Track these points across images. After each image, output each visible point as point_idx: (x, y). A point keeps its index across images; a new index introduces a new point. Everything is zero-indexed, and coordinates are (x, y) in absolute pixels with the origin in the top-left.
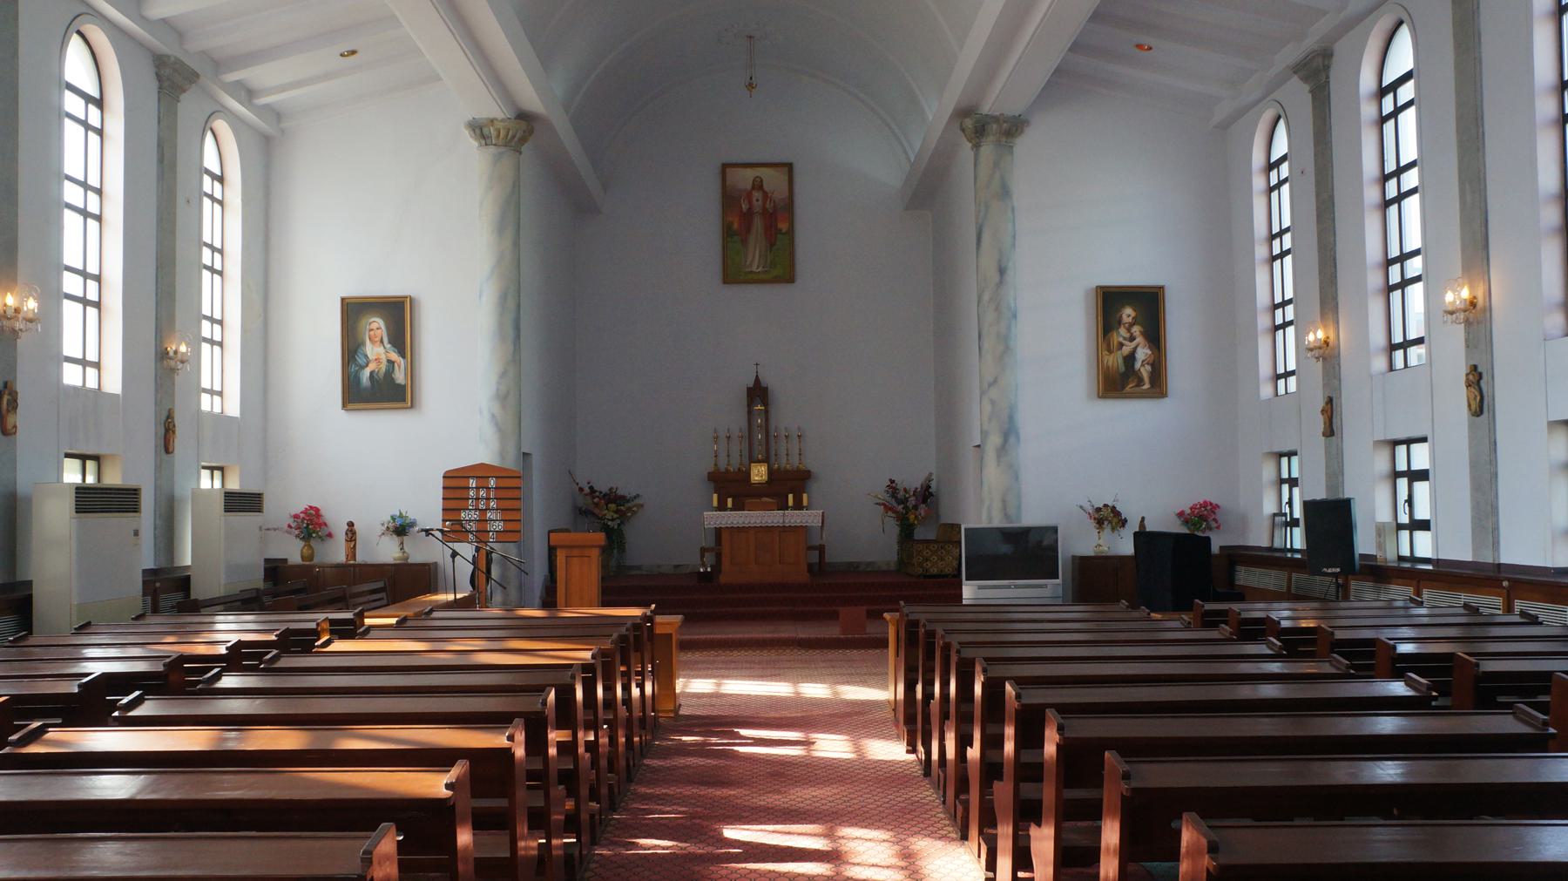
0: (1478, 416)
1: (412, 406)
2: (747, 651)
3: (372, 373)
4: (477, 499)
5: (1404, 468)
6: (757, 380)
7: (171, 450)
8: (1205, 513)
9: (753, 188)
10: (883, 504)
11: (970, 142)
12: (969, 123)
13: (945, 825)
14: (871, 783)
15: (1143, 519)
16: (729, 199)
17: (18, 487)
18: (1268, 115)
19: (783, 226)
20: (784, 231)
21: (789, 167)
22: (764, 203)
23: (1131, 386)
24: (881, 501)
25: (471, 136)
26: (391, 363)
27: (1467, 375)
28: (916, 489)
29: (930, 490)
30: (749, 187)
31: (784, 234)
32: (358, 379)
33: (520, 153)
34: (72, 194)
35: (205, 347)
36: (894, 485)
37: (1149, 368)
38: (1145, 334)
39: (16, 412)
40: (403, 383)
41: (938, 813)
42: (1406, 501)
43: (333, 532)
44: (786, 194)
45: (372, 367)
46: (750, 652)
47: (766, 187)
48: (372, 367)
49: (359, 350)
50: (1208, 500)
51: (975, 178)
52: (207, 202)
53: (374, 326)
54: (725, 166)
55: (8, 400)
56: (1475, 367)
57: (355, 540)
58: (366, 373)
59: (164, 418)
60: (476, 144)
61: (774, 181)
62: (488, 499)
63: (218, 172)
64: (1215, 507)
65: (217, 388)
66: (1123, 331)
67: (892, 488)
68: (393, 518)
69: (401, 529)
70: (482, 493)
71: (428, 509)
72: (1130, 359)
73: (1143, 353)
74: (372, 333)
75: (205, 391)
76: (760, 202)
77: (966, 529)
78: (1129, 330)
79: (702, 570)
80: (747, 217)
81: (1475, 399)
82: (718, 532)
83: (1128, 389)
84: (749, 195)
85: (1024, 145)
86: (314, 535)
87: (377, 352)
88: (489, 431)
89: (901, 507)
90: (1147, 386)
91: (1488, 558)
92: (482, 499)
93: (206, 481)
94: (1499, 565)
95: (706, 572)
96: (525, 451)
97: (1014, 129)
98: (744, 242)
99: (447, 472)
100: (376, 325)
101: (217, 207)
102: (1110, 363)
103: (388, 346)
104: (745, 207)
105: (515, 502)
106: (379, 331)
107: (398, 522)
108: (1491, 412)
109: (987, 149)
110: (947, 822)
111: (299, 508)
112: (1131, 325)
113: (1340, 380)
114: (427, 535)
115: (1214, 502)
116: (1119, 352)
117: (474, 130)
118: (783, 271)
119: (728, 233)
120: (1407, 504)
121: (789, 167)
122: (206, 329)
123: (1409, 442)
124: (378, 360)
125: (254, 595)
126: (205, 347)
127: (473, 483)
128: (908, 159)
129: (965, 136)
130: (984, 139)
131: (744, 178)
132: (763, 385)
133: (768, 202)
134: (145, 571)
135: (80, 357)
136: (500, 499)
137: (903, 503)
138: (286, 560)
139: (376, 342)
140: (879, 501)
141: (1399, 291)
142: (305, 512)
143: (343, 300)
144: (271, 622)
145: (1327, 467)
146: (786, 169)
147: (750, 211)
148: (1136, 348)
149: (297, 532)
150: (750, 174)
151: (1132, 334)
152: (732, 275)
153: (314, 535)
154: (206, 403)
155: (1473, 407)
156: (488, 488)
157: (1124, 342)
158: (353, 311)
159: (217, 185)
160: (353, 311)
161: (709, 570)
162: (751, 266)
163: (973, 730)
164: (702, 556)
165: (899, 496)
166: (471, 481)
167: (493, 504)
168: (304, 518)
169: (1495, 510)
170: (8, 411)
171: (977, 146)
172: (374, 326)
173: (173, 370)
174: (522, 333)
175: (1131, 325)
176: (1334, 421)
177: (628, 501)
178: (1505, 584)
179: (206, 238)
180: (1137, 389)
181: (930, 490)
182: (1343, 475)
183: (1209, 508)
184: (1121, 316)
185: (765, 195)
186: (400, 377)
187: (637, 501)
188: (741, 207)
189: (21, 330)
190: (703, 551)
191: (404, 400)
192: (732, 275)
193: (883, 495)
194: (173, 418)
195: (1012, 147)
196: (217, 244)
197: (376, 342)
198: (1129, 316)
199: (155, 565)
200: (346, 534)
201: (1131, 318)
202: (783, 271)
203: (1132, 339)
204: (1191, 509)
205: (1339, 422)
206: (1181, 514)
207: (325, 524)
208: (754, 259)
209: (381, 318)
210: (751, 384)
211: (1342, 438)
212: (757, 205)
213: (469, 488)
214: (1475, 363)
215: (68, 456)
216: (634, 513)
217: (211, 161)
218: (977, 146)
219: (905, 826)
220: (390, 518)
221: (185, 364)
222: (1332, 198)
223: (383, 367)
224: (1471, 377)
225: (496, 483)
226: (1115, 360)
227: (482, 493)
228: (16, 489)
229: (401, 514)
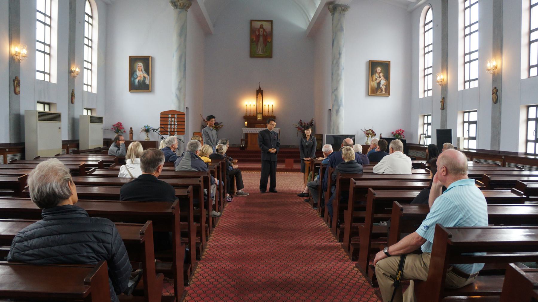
0: (496, 103)
1: (150, 92)
2: (256, 172)
3: (139, 80)
4: (171, 121)
5: (467, 120)
6: (260, 88)
7: (73, 102)
8: (400, 133)
9: (260, 28)
10: (298, 127)
11: (331, 13)
12: (331, 6)
13: (332, 236)
14: (303, 219)
15: (381, 134)
16: (253, 31)
17: (21, 110)
18: (426, 7)
19: (269, 40)
20: (269, 41)
21: (272, 21)
22: (263, 33)
23: (379, 92)
24: (297, 127)
25: (172, 6)
26: (144, 77)
27: (493, 90)
28: (308, 123)
29: (312, 124)
30: (259, 27)
31: (269, 42)
32: (134, 82)
33: (187, 11)
34: (39, 16)
35: (85, 70)
36: (301, 122)
37: (385, 87)
38: (384, 76)
39: (19, 87)
40: (148, 84)
41: (329, 231)
42: (534, 131)
43: (126, 130)
44: (270, 30)
45: (139, 78)
46: (254, 172)
47: (264, 28)
48: (139, 78)
49: (135, 73)
50: (401, 129)
51: (332, 24)
52: (86, 23)
53: (140, 65)
54: (252, 21)
55: (17, 83)
56: (495, 88)
57: (132, 133)
58: (137, 81)
59: (71, 92)
60: (173, 8)
61: (267, 26)
62: (174, 121)
63: (90, 14)
64: (403, 131)
65: (89, 84)
66: (377, 75)
67: (301, 122)
68: (145, 127)
69: (147, 131)
70: (173, 119)
71: (156, 124)
72: (379, 83)
73: (383, 82)
74: (139, 68)
75: (85, 84)
76: (262, 32)
77: (326, 135)
78: (379, 75)
79: (241, 146)
80: (258, 37)
81: (495, 98)
82: (247, 135)
83: (378, 93)
84: (259, 30)
85: (348, 14)
86: (120, 131)
87: (140, 74)
88: (175, 99)
89: (303, 128)
90: (384, 92)
91: (496, 149)
92: (176, 125)
93: (85, 112)
94: (500, 151)
95: (243, 147)
96: (187, 107)
97: (345, 9)
98: (257, 44)
99: (162, 112)
100: (140, 65)
101: (90, 26)
102: (373, 85)
103: (144, 72)
104: (257, 33)
105: (182, 122)
106: (141, 67)
107: (146, 129)
108: (500, 102)
109: (336, 15)
110: (333, 235)
111: (115, 123)
112: (380, 73)
113: (447, 92)
114: (154, 131)
115: (403, 130)
116: (376, 81)
117: (173, 3)
118: (268, 54)
119: (252, 41)
120: (535, 132)
121: (272, 21)
122: (86, 65)
123: (428, 116)
124: (140, 76)
125: (99, 149)
126: (85, 70)
127: (170, 116)
128: (309, 21)
129: (330, 11)
130: (336, 12)
131: (257, 25)
132: (262, 89)
133: (265, 32)
134: (63, 141)
135: (43, 71)
136: (179, 121)
137: (304, 127)
138: (111, 139)
139: (140, 70)
140: (296, 126)
141: (469, 63)
142: (117, 124)
143: (130, 57)
144: (484, 167)
145: (441, 119)
146: (270, 22)
147: (259, 34)
148: (381, 80)
149: (114, 130)
150: (259, 24)
151: (380, 76)
152: (253, 55)
153: (120, 131)
154: (85, 88)
155: (494, 101)
156: (175, 118)
157: (377, 78)
158: (133, 60)
159: (90, 19)
160: (133, 60)
161: (244, 146)
162: (259, 52)
163: (211, 161)
164: (241, 142)
165: (303, 125)
166: (169, 115)
167: (176, 123)
168: (117, 126)
169: (499, 133)
170: (17, 86)
171: (333, 14)
172: (140, 65)
173: (74, 77)
174: (186, 69)
175: (380, 73)
176: (445, 105)
177: (219, 124)
178: (503, 157)
179: (86, 35)
180: (381, 93)
181: (312, 124)
182: (447, 122)
183: (401, 131)
184: (377, 70)
185: (264, 30)
186: (147, 82)
187: (221, 124)
188: (256, 34)
189: (21, 60)
190: (242, 140)
191: (148, 89)
192: (253, 55)
193: (298, 125)
194: (74, 92)
195: (344, 15)
196: (90, 38)
197: (140, 70)
198: (379, 70)
199: (68, 139)
200: (130, 131)
201: (380, 71)
202: (268, 54)
203: (380, 77)
204: (396, 131)
205: (446, 105)
206: (393, 133)
207: (123, 128)
208: (260, 49)
209: (143, 64)
210: (258, 89)
211: (447, 110)
212: (261, 33)
213: (177, 125)
214: (496, 86)
215: (38, 102)
216: (221, 128)
217: (88, 10)
218: (333, 14)
219: (318, 236)
220: (144, 127)
221: (78, 75)
222: (447, 34)
223: (142, 79)
224: (494, 91)
225: (177, 116)
226: (374, 84)
227: (173, 119)
228: (20, 112)
229: (147, 125)
